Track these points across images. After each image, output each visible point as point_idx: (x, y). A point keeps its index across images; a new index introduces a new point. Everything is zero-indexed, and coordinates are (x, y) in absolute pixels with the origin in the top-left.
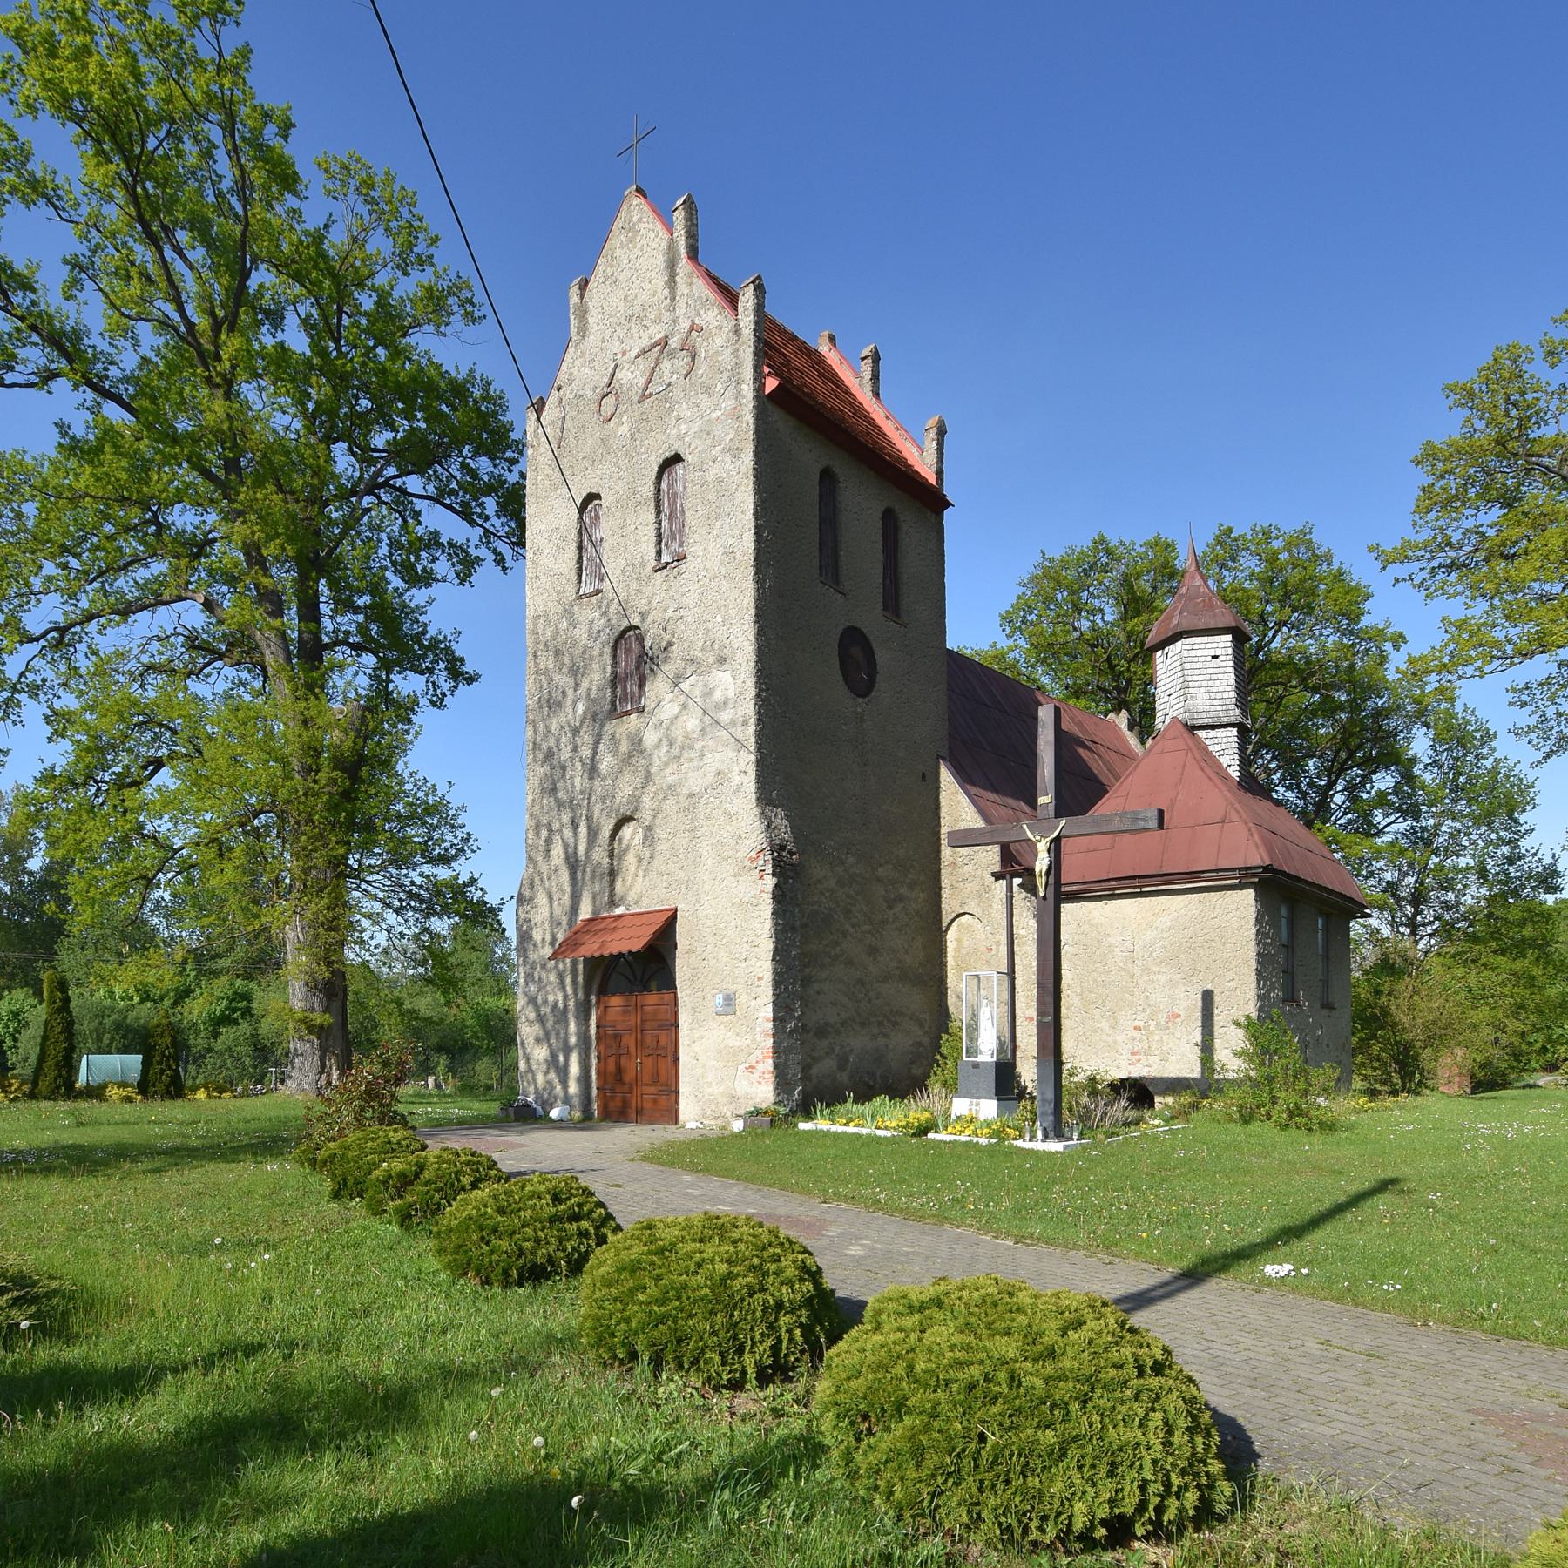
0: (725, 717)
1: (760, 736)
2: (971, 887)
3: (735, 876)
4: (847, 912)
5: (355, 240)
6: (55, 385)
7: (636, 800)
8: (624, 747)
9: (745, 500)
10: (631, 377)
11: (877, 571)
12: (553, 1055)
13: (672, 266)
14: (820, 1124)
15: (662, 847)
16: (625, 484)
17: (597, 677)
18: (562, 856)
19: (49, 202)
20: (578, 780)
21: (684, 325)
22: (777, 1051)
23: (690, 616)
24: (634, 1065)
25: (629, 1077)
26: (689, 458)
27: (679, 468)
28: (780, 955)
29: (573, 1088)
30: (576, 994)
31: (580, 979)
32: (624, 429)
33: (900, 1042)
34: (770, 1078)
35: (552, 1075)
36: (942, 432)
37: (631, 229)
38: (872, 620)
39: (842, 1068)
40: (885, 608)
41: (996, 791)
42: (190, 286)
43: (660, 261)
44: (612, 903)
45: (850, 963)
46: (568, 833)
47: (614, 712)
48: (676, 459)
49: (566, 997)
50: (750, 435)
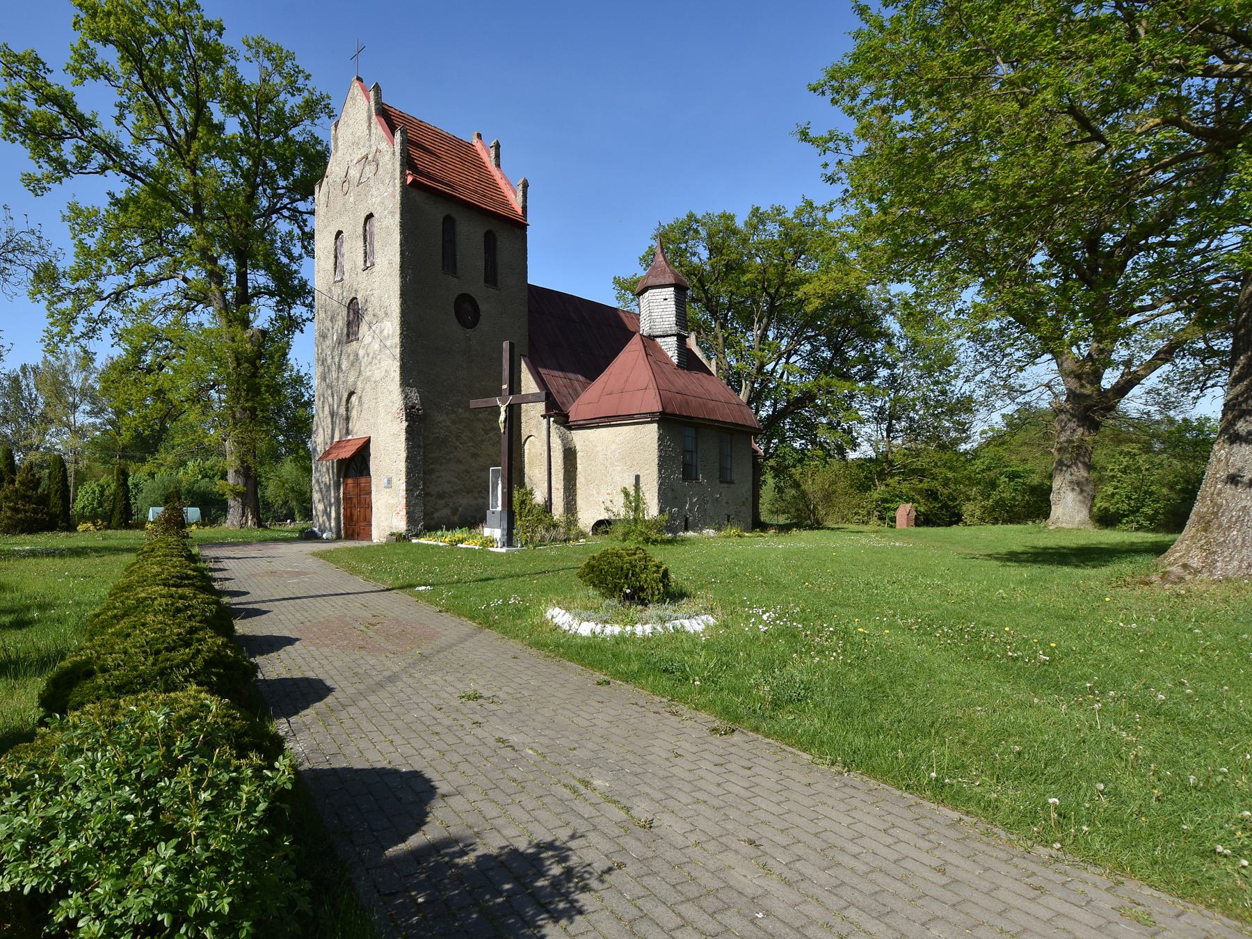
0: (388, 343)
1: (402, 354)
2: (534, 422)
4: (458, 437)
5: (264, 80)
6: (108, 172)
7: (355, 383)
8: (352, 358)
9: (397, 237)
10: (354, 173)
11: (481, 264)
13: (370, 118)
14: (423, 541)
15: (365, 406)
16: (352, 229)
17: (340, 323)
19: (106, 78)
20: (334, 375)
21: (374, 149)
22: (408, 505)
23: (376, 293)
24: (356, 512)
25: (355, 518)
26: (376, 215)
27: (374, 220)
28: (410, 459)
29: (333, 524)
32: (352, 199)
33: (465, 501)
34: (405, 518)
36: (525, 186)
37: (353, 99)
38: (478, 290)
39: (454, 513)
40: (486, 281)
41: (562, 370)
42: (174, 118)
43: (365, 115)
44: (348, 433)
45: (460, 462)
46: (330, 399)
47: (349, 341)
48: (370, 216)
50: (398, 206)
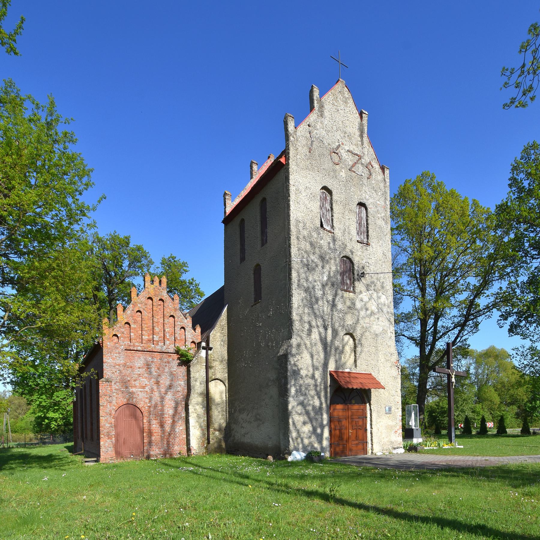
3: (391, 367)
12: (315, 429)
18: (318, 337)
25: (345, 437)
30: (326, 401)
31: (329, 395)
35: (313, 439)
46: (322, 330)
49: (321, 404)
